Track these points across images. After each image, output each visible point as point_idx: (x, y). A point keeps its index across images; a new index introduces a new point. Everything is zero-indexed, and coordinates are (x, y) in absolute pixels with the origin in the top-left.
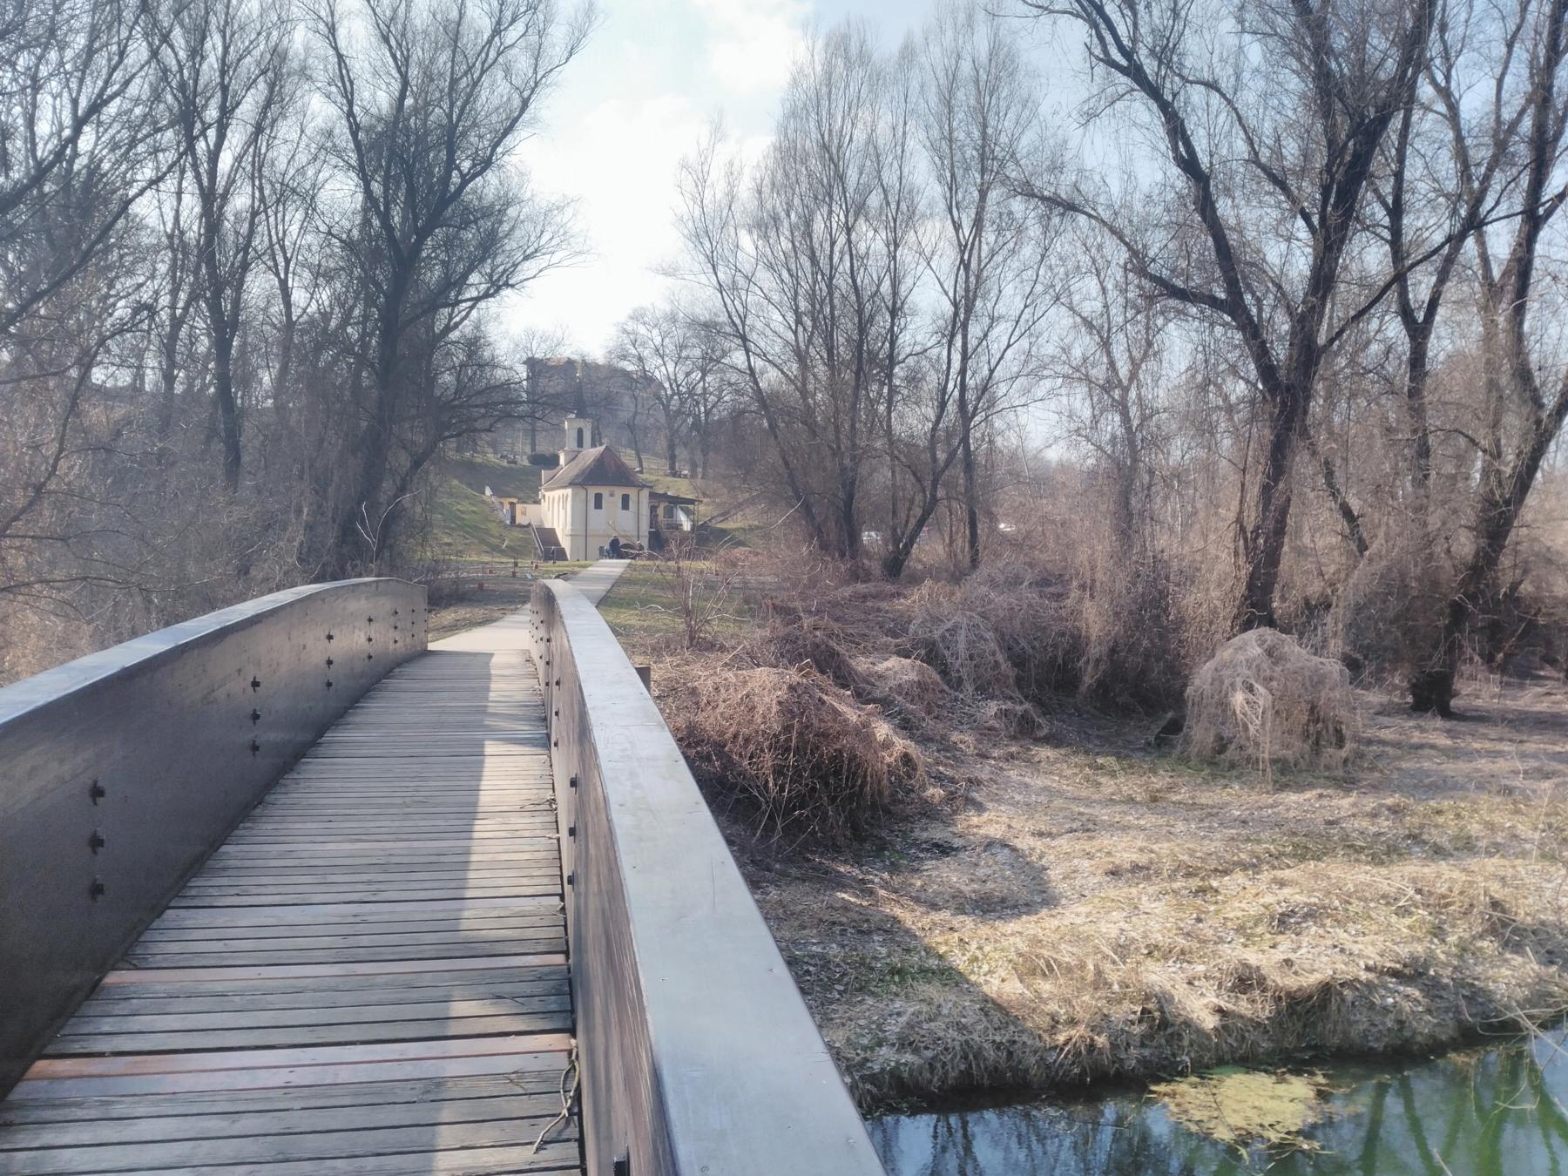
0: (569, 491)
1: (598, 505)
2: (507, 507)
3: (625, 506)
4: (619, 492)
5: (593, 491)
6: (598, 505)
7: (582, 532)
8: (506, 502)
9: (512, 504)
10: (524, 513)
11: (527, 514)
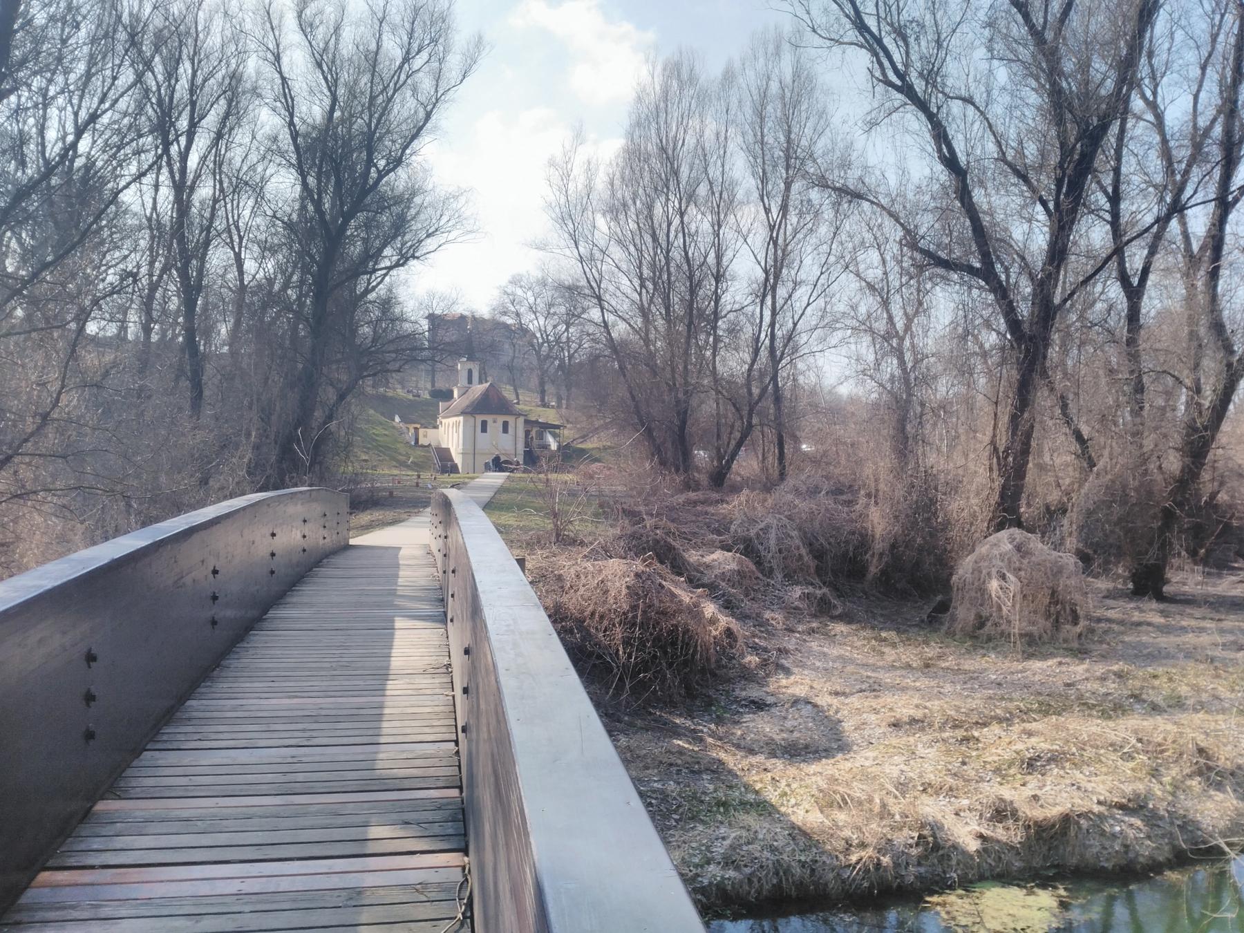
0: (461, 418)
1: (484, 430)
2: (412, 431)
3: (505, 430)
4: (501, 419)
5: (480, 418)
6: (484, 430)
7: (471, 451)
8: (411, 427)
9: (416, 429)
10: (425, 436)
11: (428, 437)
